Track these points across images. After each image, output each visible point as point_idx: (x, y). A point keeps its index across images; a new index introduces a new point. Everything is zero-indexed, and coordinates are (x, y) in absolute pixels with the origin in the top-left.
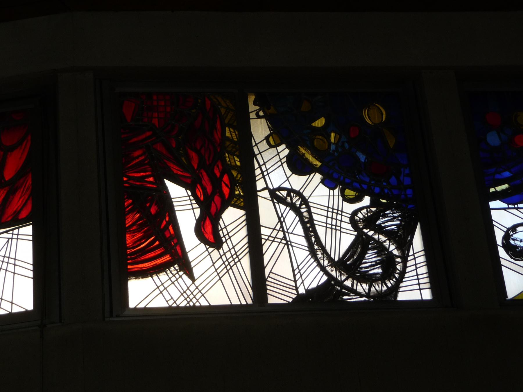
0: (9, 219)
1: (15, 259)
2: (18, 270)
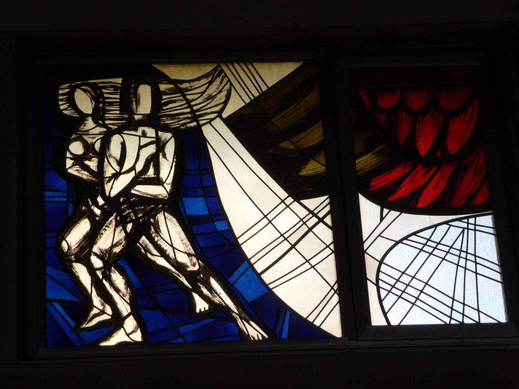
0: (462, 203)
1: (288, 206)
2: (481, 270)
